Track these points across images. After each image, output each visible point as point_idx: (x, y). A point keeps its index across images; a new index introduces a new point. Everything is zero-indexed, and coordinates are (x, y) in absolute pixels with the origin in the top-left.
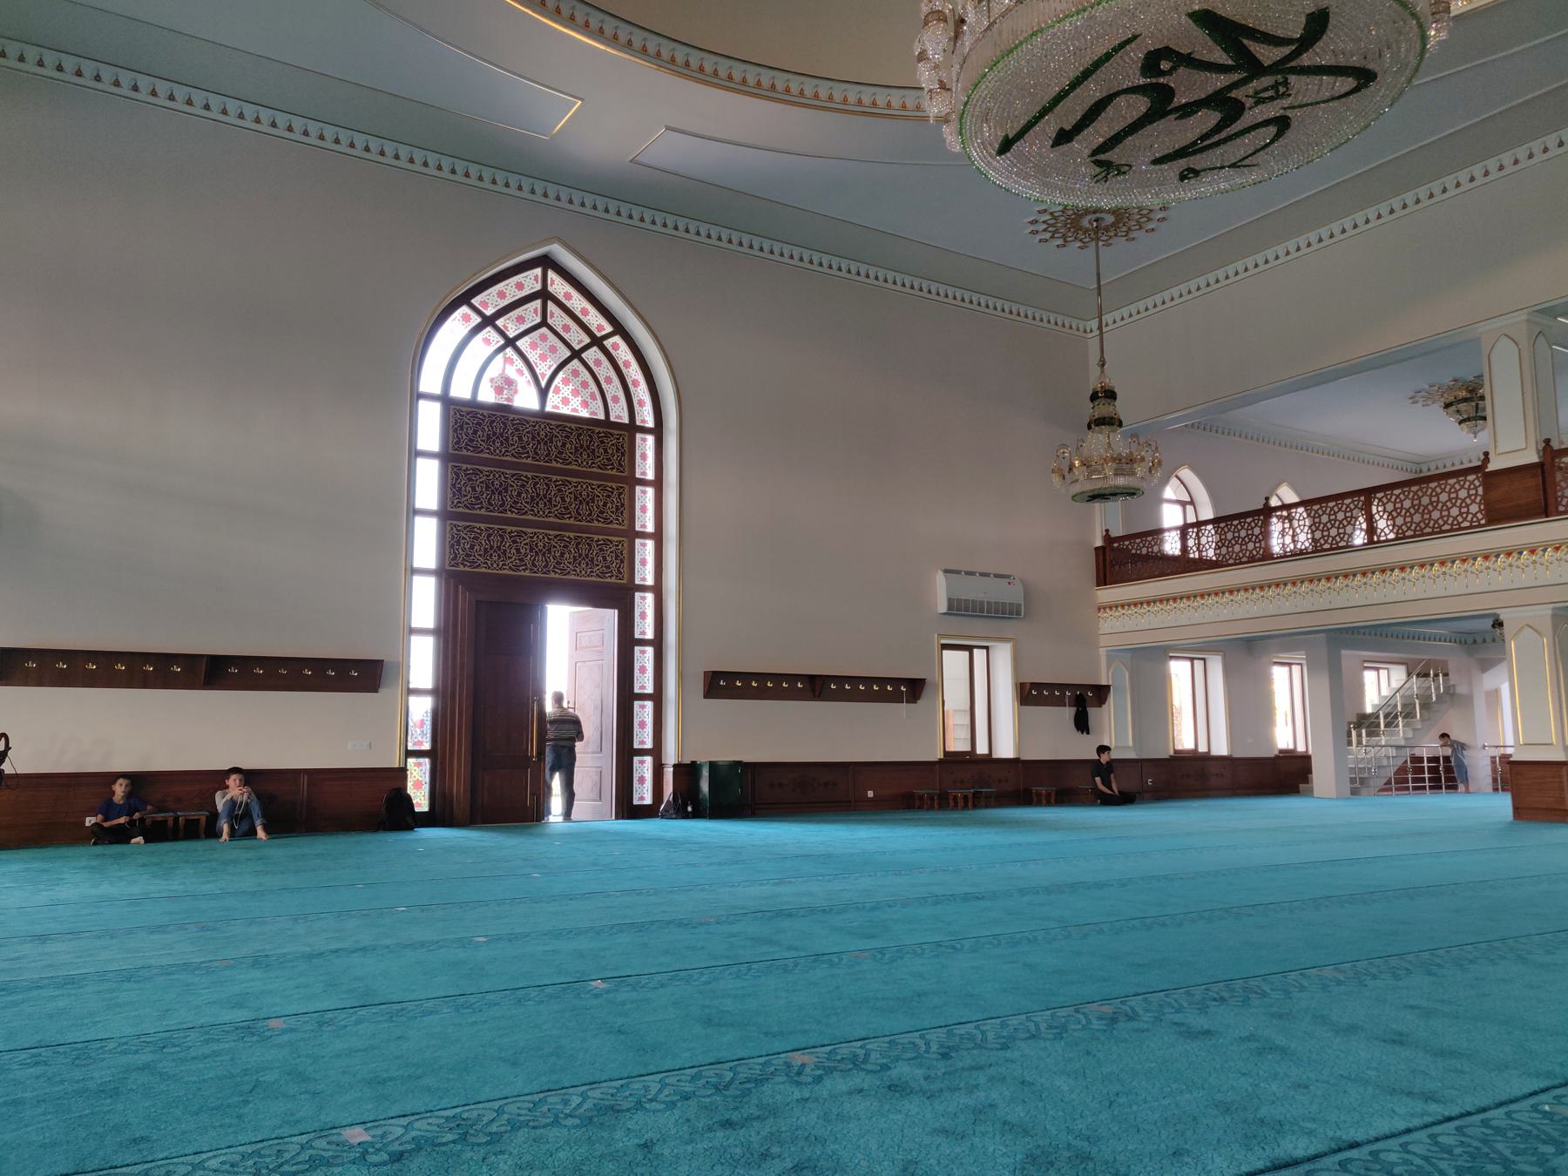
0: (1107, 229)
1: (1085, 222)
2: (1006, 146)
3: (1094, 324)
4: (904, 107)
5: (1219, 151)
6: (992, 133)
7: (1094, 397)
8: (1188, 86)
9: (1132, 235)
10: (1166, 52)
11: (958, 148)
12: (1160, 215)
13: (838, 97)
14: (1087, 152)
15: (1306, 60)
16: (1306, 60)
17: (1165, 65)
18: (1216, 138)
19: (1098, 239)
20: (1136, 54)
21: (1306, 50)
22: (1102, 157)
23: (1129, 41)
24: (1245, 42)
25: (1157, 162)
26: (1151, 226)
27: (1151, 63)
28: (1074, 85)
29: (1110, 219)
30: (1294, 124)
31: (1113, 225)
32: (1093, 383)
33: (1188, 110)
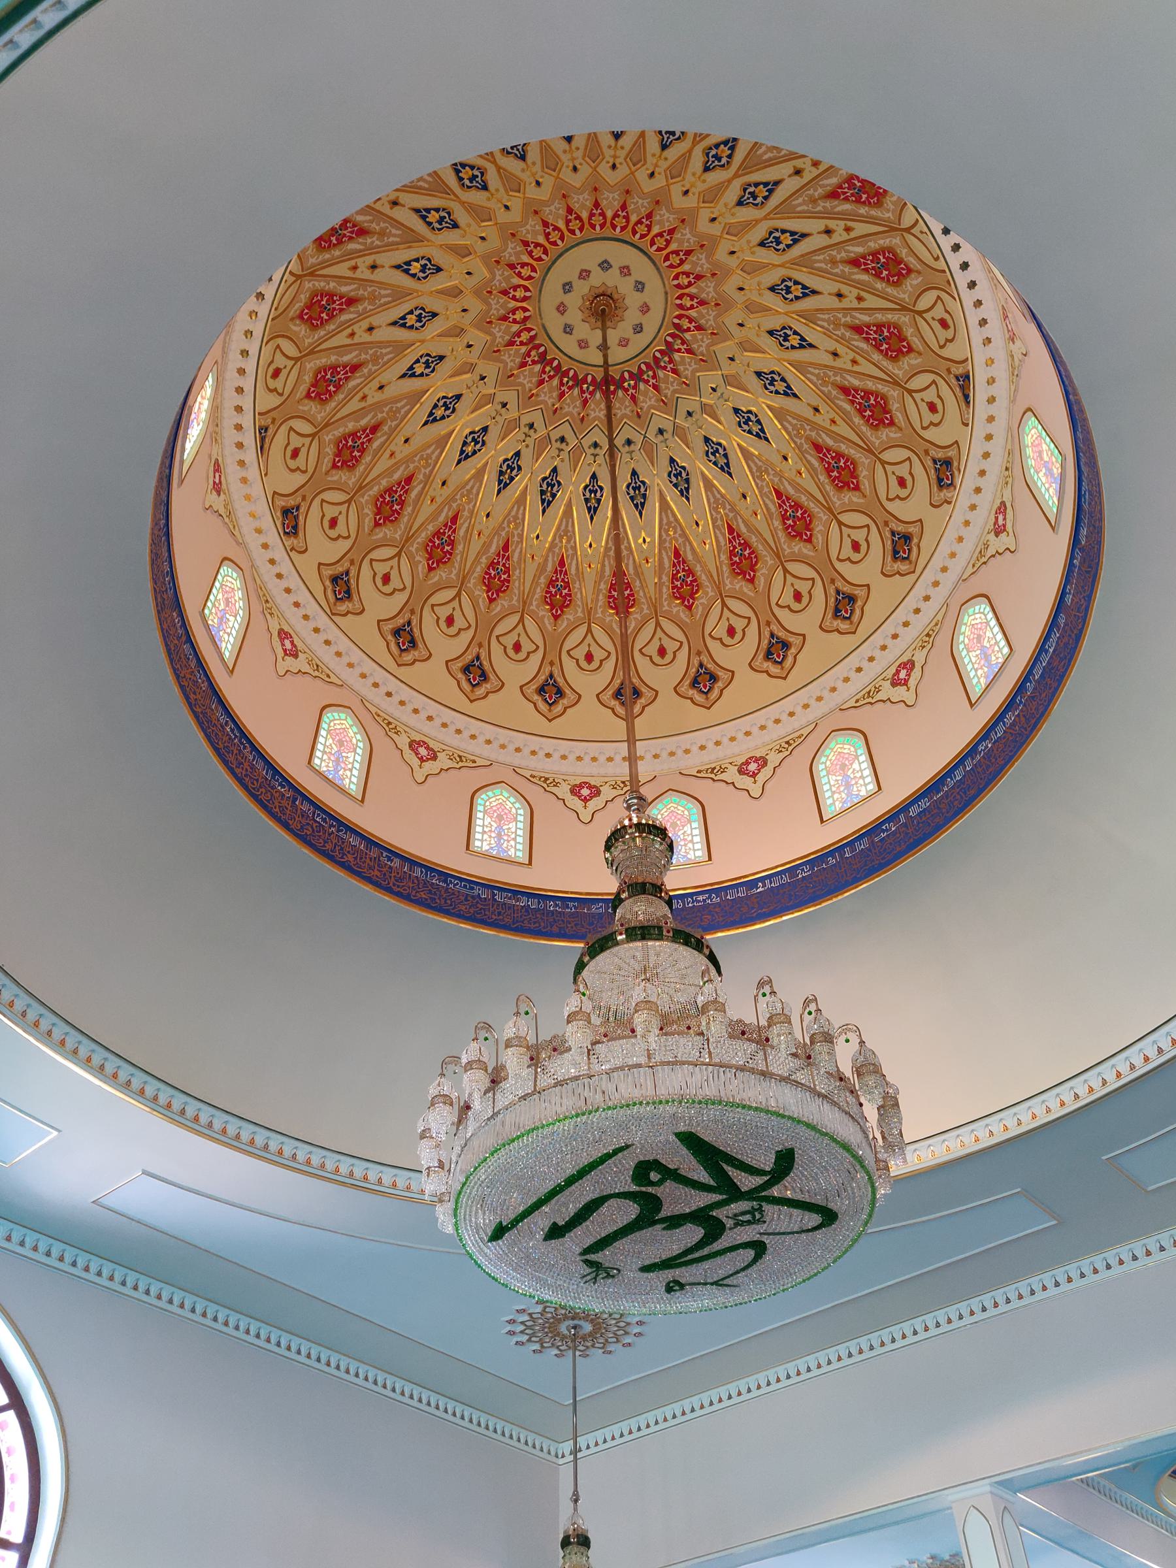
0: (584, 1338)
1: (563, 1328)
2: (499, 1232)
3: (567, 1447)
4: (394, 1185)
5: (706, 1265)
6: (487, 1220)
7: (566, 1543)
8: (677, 1199)
9: (610, 1348)
10: (656, 1165)
11: (450, 1229)
12: (637, 1330)
13: (330, 1166)
14: (578, 1250)
15: (775, 1192)
16: (775, 1192)
17: (654, 1176)
18: (697, 1255)
19: (575, 1349)
20: (627, 1162)
21: (777, 1183)
22: (592, 1257)
23: (621, 1149)
24: (725, 1166)
25: (646, 1269)
26: (627, 1340)
27: (643, 1170)
28: (571, 1181)
29: (588, 1327)
30: (770, 1250)
31: (590, 1334)
32: (563, 1526)
33: (675, 1222)
